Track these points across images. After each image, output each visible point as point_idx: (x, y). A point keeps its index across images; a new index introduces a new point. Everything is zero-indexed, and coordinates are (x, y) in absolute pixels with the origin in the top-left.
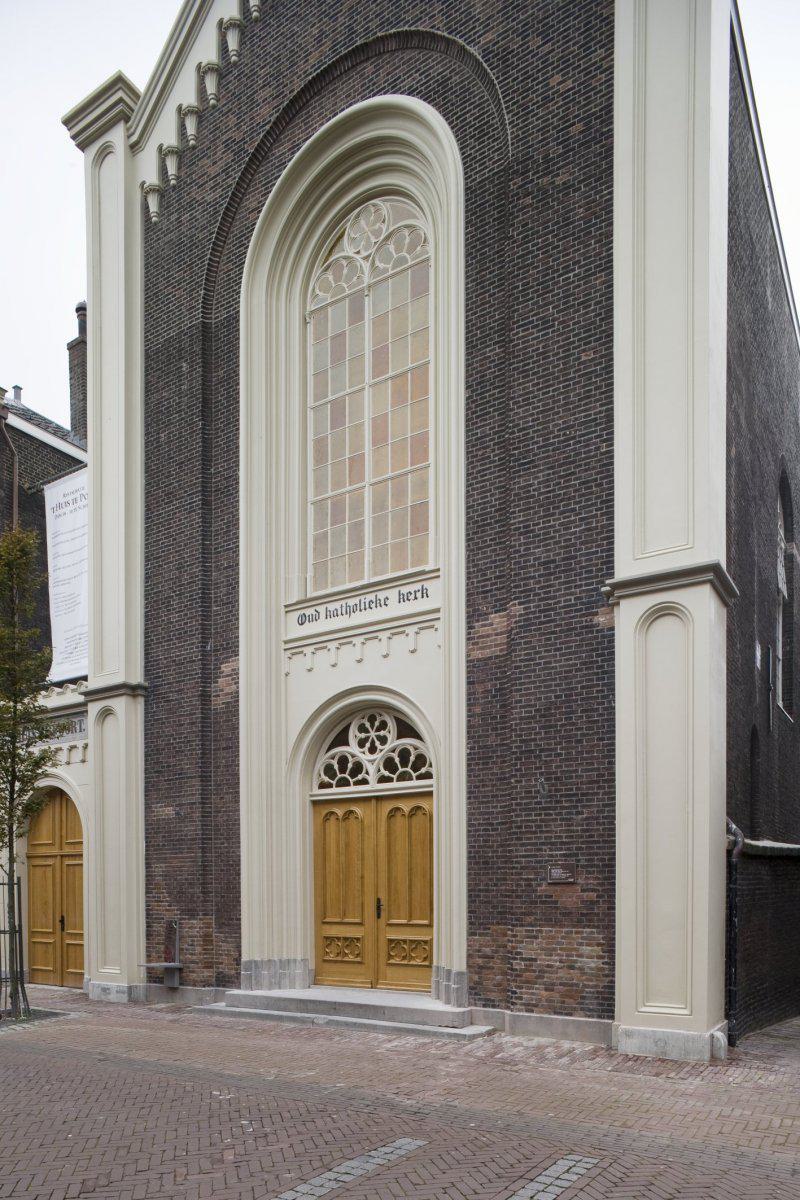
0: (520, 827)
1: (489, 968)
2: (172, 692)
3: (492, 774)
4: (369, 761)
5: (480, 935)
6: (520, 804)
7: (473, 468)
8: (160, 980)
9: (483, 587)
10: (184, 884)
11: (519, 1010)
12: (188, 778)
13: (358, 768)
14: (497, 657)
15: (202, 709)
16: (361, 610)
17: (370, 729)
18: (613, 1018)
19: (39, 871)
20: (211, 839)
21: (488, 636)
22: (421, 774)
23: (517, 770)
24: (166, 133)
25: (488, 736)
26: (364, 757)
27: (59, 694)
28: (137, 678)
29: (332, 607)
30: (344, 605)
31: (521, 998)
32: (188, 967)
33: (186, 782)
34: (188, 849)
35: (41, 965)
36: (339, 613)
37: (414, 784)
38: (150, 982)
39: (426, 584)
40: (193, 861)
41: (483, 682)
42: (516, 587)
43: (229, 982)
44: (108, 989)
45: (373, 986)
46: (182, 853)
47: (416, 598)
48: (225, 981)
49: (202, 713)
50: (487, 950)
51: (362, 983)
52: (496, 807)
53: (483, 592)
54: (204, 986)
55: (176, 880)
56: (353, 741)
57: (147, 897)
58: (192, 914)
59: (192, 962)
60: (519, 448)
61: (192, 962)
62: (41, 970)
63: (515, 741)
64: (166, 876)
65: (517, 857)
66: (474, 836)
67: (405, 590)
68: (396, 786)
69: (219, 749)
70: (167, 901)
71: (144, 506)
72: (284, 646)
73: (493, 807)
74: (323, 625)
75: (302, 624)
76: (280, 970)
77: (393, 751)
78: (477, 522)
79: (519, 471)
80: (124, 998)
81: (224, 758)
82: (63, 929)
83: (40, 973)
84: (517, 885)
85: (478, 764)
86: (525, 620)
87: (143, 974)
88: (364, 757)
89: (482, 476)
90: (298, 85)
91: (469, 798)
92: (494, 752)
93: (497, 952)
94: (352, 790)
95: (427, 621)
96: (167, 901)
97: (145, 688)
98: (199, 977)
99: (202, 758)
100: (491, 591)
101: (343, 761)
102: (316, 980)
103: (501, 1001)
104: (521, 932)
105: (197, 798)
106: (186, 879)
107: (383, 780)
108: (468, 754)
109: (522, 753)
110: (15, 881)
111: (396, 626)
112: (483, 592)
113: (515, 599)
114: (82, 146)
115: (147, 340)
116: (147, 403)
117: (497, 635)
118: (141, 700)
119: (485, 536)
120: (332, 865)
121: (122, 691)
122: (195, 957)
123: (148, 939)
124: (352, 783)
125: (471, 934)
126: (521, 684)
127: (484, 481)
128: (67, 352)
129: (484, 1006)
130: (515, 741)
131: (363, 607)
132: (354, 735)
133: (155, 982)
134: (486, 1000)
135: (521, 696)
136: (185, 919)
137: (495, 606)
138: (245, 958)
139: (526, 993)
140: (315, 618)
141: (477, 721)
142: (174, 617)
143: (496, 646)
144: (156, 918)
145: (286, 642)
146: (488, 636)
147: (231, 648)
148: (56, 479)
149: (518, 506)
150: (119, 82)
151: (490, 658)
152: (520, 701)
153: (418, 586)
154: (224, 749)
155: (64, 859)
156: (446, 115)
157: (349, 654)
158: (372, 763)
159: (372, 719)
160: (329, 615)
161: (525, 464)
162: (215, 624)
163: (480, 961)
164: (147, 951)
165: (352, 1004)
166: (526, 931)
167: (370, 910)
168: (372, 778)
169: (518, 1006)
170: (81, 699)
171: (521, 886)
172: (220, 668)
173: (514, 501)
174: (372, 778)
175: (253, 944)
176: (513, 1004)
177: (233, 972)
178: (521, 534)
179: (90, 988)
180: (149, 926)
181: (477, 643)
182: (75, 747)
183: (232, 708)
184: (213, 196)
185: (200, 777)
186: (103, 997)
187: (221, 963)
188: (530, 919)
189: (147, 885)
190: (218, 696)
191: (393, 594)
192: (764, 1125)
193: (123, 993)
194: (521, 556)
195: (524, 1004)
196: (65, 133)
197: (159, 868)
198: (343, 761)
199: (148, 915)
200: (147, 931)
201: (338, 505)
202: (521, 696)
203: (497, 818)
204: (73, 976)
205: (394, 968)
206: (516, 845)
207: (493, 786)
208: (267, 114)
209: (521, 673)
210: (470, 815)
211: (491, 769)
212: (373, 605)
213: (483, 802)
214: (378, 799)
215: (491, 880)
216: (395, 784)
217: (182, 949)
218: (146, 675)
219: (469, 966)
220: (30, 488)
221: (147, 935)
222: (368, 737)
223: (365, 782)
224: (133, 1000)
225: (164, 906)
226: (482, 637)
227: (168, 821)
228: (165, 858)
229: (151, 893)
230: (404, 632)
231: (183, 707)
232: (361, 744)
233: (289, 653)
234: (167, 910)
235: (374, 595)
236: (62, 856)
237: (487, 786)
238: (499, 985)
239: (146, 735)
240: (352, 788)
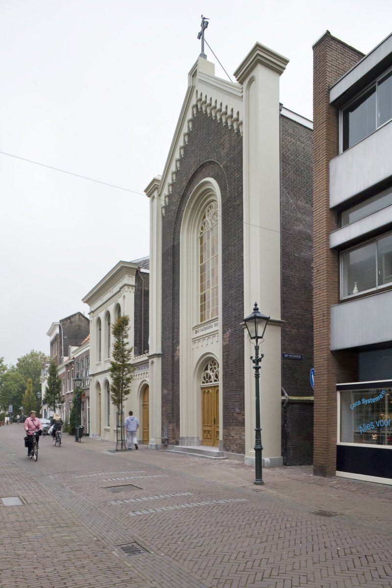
18: (244, 453)
24: (166, 192)
26: (211, 374)
48: (177, 443)
56: (209, 369)
58: (170, 422)
72: (192, 340)
76: (190, 440)
80: (155, 448)
88: (211, 374)
90: (190, 176)
95: (214, 334)
101: (207, 375)
102: (202, 443)
105: (171, 388)
114: (149, 196)
118: (161, 358)
120: (206, 408)
132: (209, 367)
147: (178, 342)
150: (154, 180)
156: (218, 183)
167: (213, 422)
170: (147, 358)
175: (183, 433)
184: (175, 208)
188: (233, 424)
196: (145, 194)
208: (185, 184)
219: (223, 439)
223: (211, 382)
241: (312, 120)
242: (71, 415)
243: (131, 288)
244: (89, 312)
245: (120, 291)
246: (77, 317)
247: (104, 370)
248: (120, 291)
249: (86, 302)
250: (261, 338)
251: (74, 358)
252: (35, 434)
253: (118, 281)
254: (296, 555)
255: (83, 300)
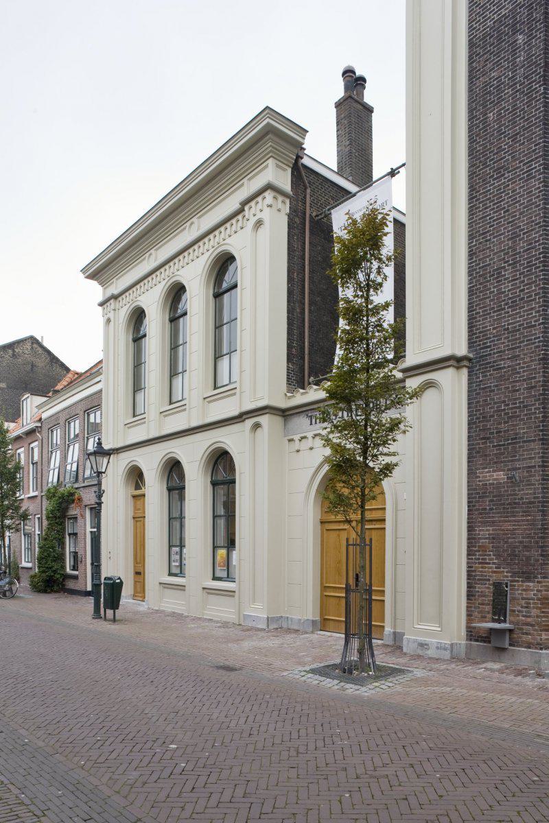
2: (504, 359)
8: (486, 639)
10: (517, 547)
12: (524, 442)
15: (544, 372)
19: (333, 535)
27: (302, 394)
28: (462, 350)
32: (522, 629)
33: (523, 447)
34: (524, 512)
35: (332, 616)
38: (471, 640)
46: (514, 516)
49: (544, 376)
54: (541, 649)
55: (506, 542)
57: (468, 559)
59: (528, 624)
61: (528, 624)
62: (332, 620)
64: (493, 538)
70: (494, 563)
71: (467, 186)
83: (331, 623)
87: (463, 633)
96: (494, 563)
97: (470, 360)
99: (543, 421)
106: (521, 542)
110: (368, 542)
115: (471, 28)
116: (470, 90)
118: (465, 371)
121: (267, 411)
122: (529, 620)
123: (468, 599)
128: (335, 110)
133: (477, 641)
136: (518, 581)
142: (506, 287)
144: (478, 580)
148: (342, 202)
164: (468, 611)
179: (405, 643)
180: (469, 586)
182: (305, 437)
185: (540, 440)
186: (420, 652)
189: (468, 547)
193: (445, 649)
197: (484, 532)
199: (470, 575)
200: (468, 591)
217: (514, 611)
218: (469, 347)
220: (317, 216)
221: (468, 596)
224: (454, 658)
225: (491, 568)
227: (498, 486)
228: (493, 522)
229: (473, 555)
231: (518, 373)
234: (495, 572)
239: (469, 404)
241: (336, 171)
242: (40, 548)
243: (280, 198)
244: (100, 299)
245: (240, 211)
246: (28, 345)
247: (157, 435)
248: (240, 211)
249: (92, 276)
250: (104, 473)
251: (40, 419)
252: (377, 470)
253: (248, 173)
254: (404, 799)
255: (83, 271)
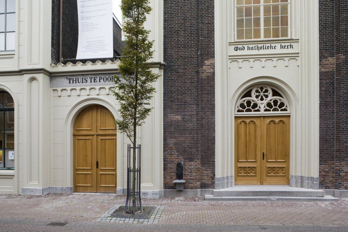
0: (344, 129)
1: (327, 176)
2: (180, 69)
3: (329, 111)
4: (261, 103)
5: (324, 164)
6: (343, 121)
7: (322, 7)
9: (326, 48)
11: (343, 189)
13: (255, 105)
14: (331, 72)
16: (264, 49)
17: (261, 92)
19: (81, 142)
20: (199, 129)
21: (327, 64)
22: (282, 109)
23: (342, 110)
25: (328, 98)
26: (259, 102)
29: (250, 46)
30: (256, 46)
31: (343, 185)
36: (254, 48)
37: (279, 113)
38: (166, 189)
39: (292, 44)
40: (192, 138)
41: (326, 80)
42: (342, 49)
43: (207, 186)
44: (147, 193)
45: (262, 184)
47: (288, 48)
50: (327, 170)
51: (256, 183)
52: (330, 122)
53: (326, 50)
59: (191, 179)
60: (343, 4)
61: (191, 179)
63: (342, 100)
65: (342, 138)
66: (322, 131)
67: (283, 45)
68: (272, 113)
69: (204, 94)
70: (176, 155)
72: (228, 58)
73: (329, 122)
74: (246, 52)
75: (236, 50)
77: (280, 100)
78: (323, 25)
79: (344, 11)
81: (206, 97)
82: (97, 167)
84: (342, 148)
85: (323, 107)
86: (345, 61)
88: (259, 102)
89: (325, 11)
91: (320, 118)
92: (329, 103)
93: (330, 170)
94: (253, 113)
96: (176, 155)
98: (194, 185)
100: (329, 49)
103: (332, 186)
104: (343, 163)
106: (188, 146)
107: (266, 110)
108: (320, 103)
109: (344, 104)
111: (280, 57)
112: (326, 50)
113: (342, 53)
117: (331, 64)
119: (326, 31)
121: (42, 71)
124: (253, 111)
125: (320, 164)
126: (344, 82)
127: (325, 12)
129: (325, 188)
130: (342, 100)
131: (265, 48)
132: (254, 93)
134: (326, 186)
135: (344, 85)
136: (187, 162)
137: (330, 55)
138: (216, 176)
139: (345, 183)
140: (243, 49)
141: (323, 92)
143: (331, 68)
144: (169, 162)
145: (229, 56)
146: (327, 64)
149: (343, 23)
151: (328, 72)
152: (344, 87)
153: (289, 44)
154: (206, 94)
155: (98, 136)
157: (269, 64)
158: (262, 105)
159: (262, 89)
160: (249, 48)
161: (345, 9)
162: (201, 45)
163: (324, 173)
165: (279, 192)
166: (345, 163)
168: (262, 109)
169: (342, 188)
171: (344, 148)
172: (204, 62)
173: (341, 21)
174: (262, 109)
176: (340, 187)
177: (210, 182)
178: (344, 32)
180: (165, 165)
181: (323, 66)
183: (211, 78)
187: (204, 179)
190: (203, 73)
191: (278, 45)
192: (209, 214)
194: (344, 40)
195: (345, 187)
197: (171, 141)
198: (249, 103)
201: (248, 12)
202: (344, 85)
203: (331, 125)
204: (104, 188)
205: (270, 177)
206: (342, 134)
207: (329, 115)
209: (344, 78)
210: (320, 124)
211: (329, 109)
212: (269, 48)
213: (325, 120)
214: (264, 117)
215: (328, 146)
216: (271, 112)
219: (320, 175)
222: (260, 95)
223: (258, 111)
226: (325, 64)
227: (178, 122)
228: (176, 137)
230: (237, 61)
232: (257, 97)
233: (231, 60)
235: (270, 44)
236: (97, 135)
237: (327, 114)
238: (331, 181)
240: (253, 113)
